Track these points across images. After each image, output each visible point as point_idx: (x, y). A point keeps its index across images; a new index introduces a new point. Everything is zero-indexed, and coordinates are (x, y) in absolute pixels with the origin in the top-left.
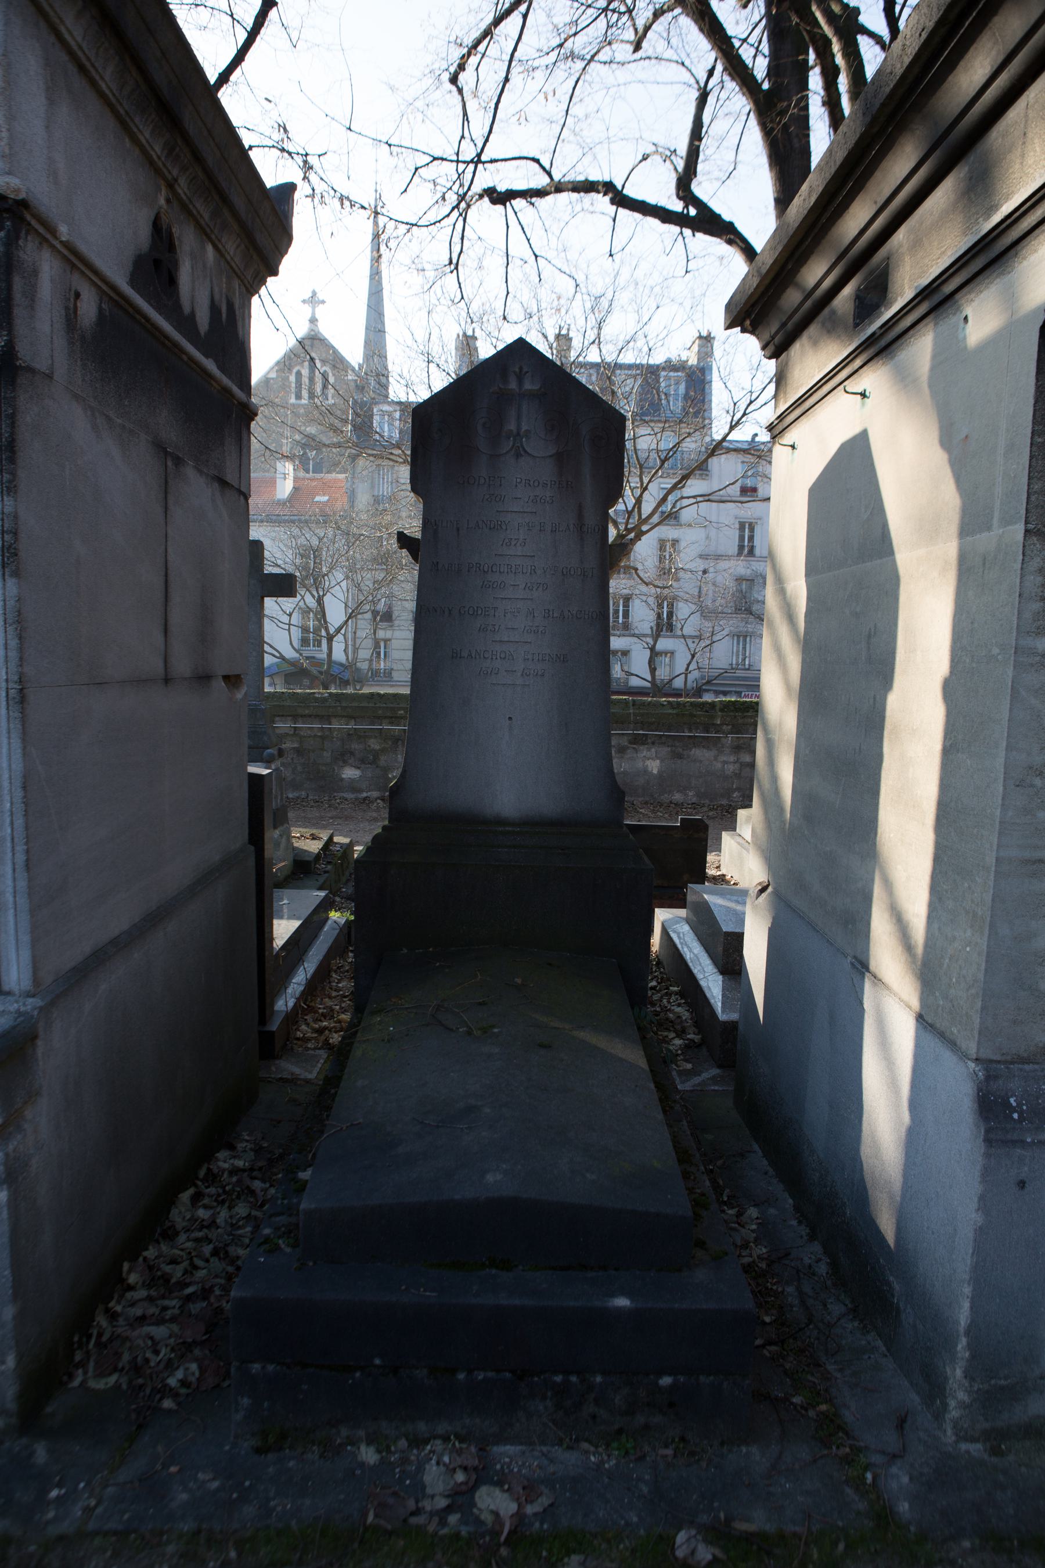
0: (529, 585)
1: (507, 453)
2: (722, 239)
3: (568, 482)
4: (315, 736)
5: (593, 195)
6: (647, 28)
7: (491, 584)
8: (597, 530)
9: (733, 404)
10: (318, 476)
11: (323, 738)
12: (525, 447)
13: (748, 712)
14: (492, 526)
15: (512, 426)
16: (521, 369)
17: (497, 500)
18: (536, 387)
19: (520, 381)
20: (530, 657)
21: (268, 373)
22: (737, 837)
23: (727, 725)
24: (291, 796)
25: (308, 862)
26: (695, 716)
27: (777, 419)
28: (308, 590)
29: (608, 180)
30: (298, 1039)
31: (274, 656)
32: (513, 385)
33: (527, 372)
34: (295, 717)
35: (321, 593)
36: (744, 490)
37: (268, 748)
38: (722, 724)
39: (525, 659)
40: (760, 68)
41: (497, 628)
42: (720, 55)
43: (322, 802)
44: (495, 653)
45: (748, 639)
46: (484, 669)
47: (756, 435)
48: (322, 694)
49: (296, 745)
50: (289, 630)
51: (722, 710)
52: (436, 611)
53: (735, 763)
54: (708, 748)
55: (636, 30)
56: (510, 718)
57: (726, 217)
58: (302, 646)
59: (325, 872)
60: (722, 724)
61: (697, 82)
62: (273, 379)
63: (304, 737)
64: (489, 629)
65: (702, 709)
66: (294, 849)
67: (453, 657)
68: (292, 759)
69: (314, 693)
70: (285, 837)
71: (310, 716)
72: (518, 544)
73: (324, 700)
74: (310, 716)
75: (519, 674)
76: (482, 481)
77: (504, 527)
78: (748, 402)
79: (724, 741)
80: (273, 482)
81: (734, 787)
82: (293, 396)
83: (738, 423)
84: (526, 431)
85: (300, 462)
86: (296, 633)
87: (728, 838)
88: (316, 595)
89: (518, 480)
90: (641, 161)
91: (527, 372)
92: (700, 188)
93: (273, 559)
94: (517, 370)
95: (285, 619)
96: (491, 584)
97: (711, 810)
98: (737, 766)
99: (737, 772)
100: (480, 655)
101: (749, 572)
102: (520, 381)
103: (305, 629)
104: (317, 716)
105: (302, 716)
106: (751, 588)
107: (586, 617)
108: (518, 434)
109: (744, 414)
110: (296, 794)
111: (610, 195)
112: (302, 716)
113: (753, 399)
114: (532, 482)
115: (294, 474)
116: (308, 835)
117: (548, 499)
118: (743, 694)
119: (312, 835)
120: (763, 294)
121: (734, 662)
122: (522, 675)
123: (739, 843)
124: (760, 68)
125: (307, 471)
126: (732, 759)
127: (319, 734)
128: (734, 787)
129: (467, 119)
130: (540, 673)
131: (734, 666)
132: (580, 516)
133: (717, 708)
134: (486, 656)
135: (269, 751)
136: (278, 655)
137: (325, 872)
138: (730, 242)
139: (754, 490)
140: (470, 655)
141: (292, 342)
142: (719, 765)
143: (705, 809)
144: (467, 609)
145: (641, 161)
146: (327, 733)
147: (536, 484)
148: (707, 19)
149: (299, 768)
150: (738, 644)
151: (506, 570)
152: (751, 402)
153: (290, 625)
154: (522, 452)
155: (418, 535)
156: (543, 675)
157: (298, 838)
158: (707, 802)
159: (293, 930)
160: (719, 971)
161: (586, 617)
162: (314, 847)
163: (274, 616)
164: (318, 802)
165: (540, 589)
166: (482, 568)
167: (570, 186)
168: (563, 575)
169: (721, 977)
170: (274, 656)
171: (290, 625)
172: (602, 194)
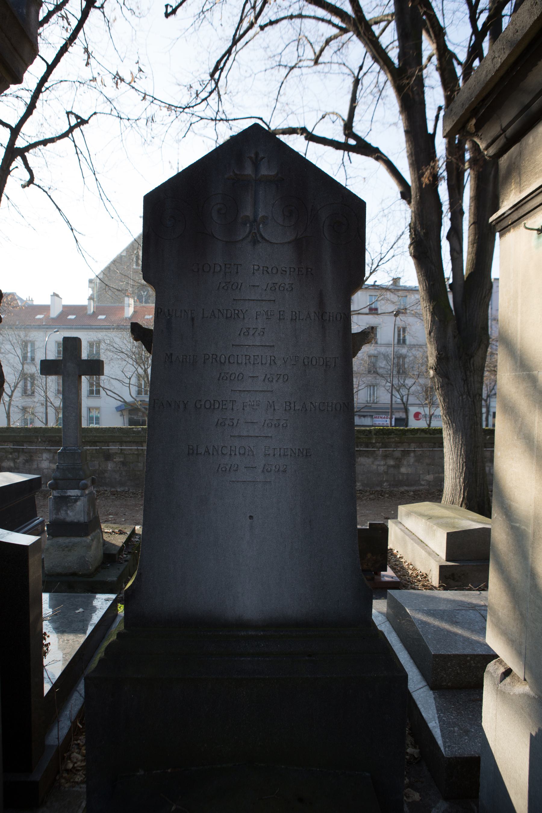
0: (268, 376)
1: (244, 239)
2: (371, 157)
3: (307, 269)
4: (133, 453)
5: (295, 136)
6: (322, 50)
7: (228, 376)
8: (339, 318)
9: (371, 261)
10: (148, 305)
11: (138, 455)
12: (263, 234)
13: (391, 435)
14: (229, 315)
15: (248, 212)
16: (257, 154)
17: (234, 287)
18: (273, 173)
19: (256, 166)
20: (271, 452)
21: (122, 253)
22: (399, 525)
23: (379, 443)
24: (119, 490)
25: (114, 555)
26: (360, 438)
27: (510, 209)
28: (139, 365)
29: (303, 126)
30: (68, 771)
31: (120, 401)
32: (249, 171)
33: (263, 158)
34: (121, 443)
35: (146, 367)
36: (371, 309)
37: (83, 480)
38: (376, 442)
39: (265, 455)
40: (394, 54)
41: (235, 422)
42: (369, 50)
43: (137, 494)
44: (233, 448)
45: (376, 388)
46: (222, 466)
47: (376, 281)
48: (138, 428)
49: (122, 460)
50: (129, 387)
51: (375, 434)
52: (170, 405)
53: (384, 465)
54: (368, 457)
55: (315, 53)
56: (251, 517)
57: (374, 145)
58: (138, 394)
59: (126, 561)
60: (376, 442)
61: (353, 73)
62: (124, 256)
63: (127, 454)
64: (227, 423)
65: (364, 433)
66: (105, 543)
67: (189, 454)
68: (120, 468)
69: (133, 428)
70: (96, 540)
71: (130, 442)
72: (256, 334)
73: (139, 432)
74: (130, 442)
75: (260, 471)
76: (218, 269)
77: (241, 316)
78: (379, 259)
79: (377, 452)
80: (122, 309)
81: (384, 479)
82: (135, 265)
83: (374, 270)
84: (263, 217)
85: (138, 298)
86: (134, 390)
87: (394, 525)
88: (143, 368)
89: (256, 267)
90: (321, 119)
91: (263, 158)
92: (358, 128)
93: (120, 349)
94: (253, 155)
95: (127, 381)
96: (228, 376)
97: (371, 494)
98: (386, 467)
99: (386, 470)
100: (217, 451)
101: (376, 352)
102: (256, 166)
103: (139, 386)
104: (134, 442)
105: (125, 442)
106: (376, 361)
107: (330, 409)
108: (255, 220)
109: (378, 266)
110: (122, 489)
111: (305, 135)
112: (125, 442)
113: (382, 257)
114: (270, 270)
115: (134, 304)
116: (117, 531)
117: (287, 286)
118: (374, 416)
119: (120, 530)
120: (502, 79)
121: (369, 400)
122: (263, 471)
123: (401, 529)
124: (394, 54)
125: (141, 302)
126: (382, 463)
127: (136, 453)
128: (384, 479)
129: (221, 100)
130: (281, 469)
131: (368, 402)
132: (321, 304)
133: (373, 433)
134: (224, 452)
135: (83, 482)
136: (123, 401)
137: (126, 561)
138: (377, 159)
139: (376, 309)
140: (207, 452)
141: (133, 239)
142: (375, 467)
143: (368, 494)
144: (203, 403)
145: (321, 119)
146: (141, 452)
147: (274, 271)
148: (363, 24)
149: (124, 473)
150: (370, 390)
151: (244, 362)
152: (381, 259)
153: (129, 384)
154: (259, 239)
155: (152, 328)
156: (285, 471)
157: (110, 533)
158: (368, 489)
159: (77, 647)
160: (428, 685)
161: (330, 409)
162: (119, 541)
163: (121, 379)
164: (135, 494)
165: (281, 380)
166: (218, 359)
167: (281, 131)
168: (305, 365)
169: (431, 692)
170: (120, 401)
171: (129, 384)
172: (299, 135)
